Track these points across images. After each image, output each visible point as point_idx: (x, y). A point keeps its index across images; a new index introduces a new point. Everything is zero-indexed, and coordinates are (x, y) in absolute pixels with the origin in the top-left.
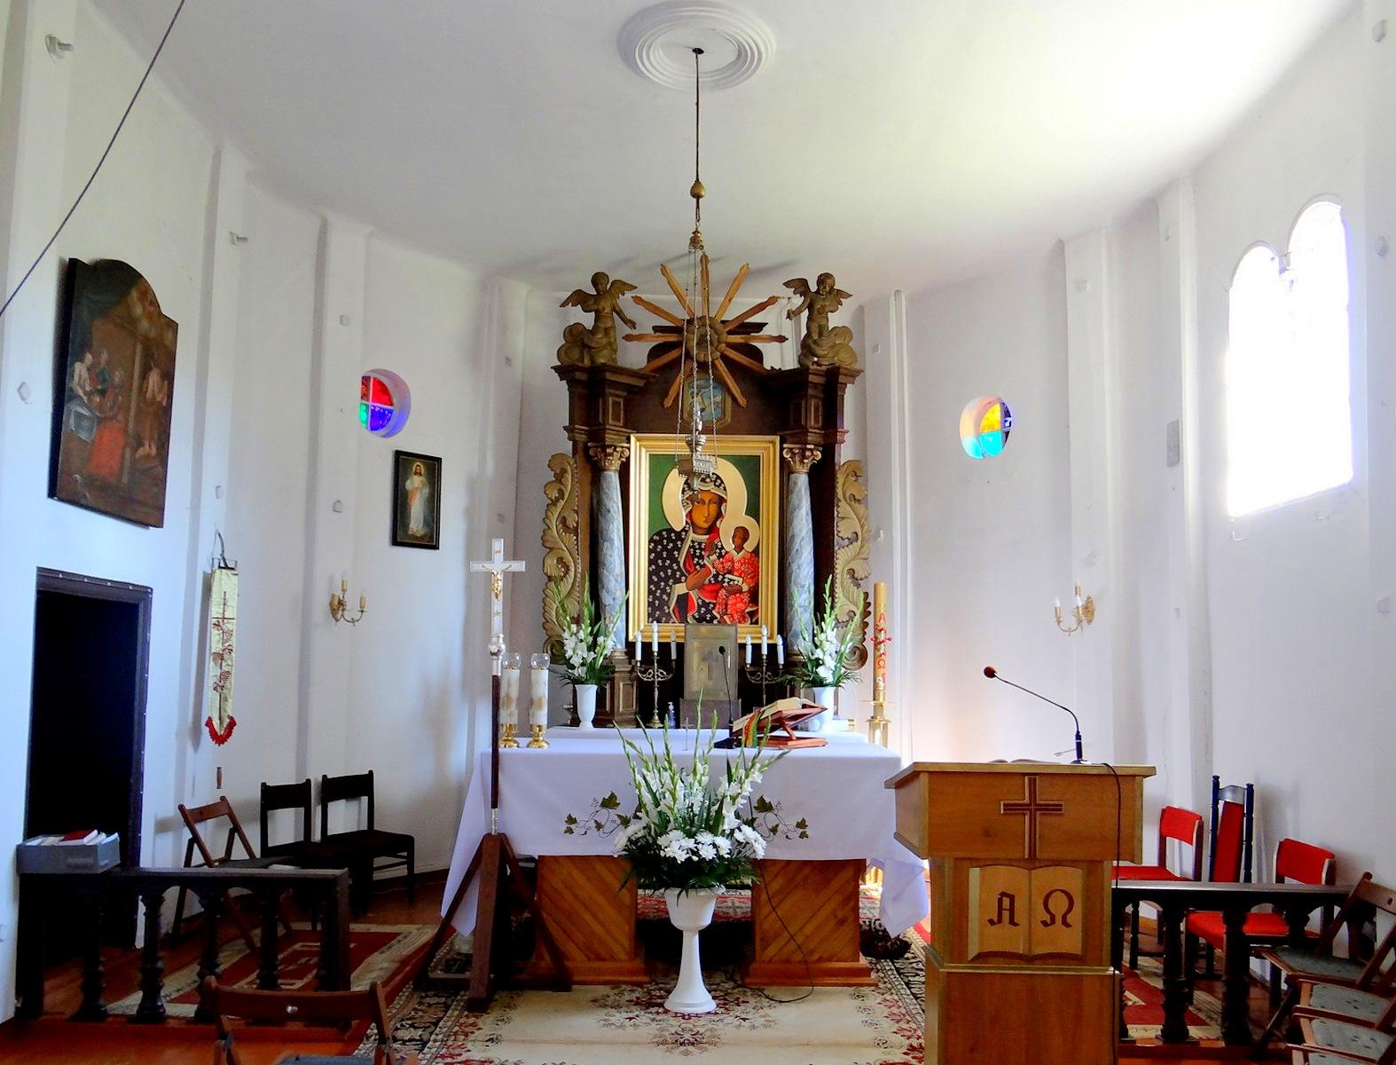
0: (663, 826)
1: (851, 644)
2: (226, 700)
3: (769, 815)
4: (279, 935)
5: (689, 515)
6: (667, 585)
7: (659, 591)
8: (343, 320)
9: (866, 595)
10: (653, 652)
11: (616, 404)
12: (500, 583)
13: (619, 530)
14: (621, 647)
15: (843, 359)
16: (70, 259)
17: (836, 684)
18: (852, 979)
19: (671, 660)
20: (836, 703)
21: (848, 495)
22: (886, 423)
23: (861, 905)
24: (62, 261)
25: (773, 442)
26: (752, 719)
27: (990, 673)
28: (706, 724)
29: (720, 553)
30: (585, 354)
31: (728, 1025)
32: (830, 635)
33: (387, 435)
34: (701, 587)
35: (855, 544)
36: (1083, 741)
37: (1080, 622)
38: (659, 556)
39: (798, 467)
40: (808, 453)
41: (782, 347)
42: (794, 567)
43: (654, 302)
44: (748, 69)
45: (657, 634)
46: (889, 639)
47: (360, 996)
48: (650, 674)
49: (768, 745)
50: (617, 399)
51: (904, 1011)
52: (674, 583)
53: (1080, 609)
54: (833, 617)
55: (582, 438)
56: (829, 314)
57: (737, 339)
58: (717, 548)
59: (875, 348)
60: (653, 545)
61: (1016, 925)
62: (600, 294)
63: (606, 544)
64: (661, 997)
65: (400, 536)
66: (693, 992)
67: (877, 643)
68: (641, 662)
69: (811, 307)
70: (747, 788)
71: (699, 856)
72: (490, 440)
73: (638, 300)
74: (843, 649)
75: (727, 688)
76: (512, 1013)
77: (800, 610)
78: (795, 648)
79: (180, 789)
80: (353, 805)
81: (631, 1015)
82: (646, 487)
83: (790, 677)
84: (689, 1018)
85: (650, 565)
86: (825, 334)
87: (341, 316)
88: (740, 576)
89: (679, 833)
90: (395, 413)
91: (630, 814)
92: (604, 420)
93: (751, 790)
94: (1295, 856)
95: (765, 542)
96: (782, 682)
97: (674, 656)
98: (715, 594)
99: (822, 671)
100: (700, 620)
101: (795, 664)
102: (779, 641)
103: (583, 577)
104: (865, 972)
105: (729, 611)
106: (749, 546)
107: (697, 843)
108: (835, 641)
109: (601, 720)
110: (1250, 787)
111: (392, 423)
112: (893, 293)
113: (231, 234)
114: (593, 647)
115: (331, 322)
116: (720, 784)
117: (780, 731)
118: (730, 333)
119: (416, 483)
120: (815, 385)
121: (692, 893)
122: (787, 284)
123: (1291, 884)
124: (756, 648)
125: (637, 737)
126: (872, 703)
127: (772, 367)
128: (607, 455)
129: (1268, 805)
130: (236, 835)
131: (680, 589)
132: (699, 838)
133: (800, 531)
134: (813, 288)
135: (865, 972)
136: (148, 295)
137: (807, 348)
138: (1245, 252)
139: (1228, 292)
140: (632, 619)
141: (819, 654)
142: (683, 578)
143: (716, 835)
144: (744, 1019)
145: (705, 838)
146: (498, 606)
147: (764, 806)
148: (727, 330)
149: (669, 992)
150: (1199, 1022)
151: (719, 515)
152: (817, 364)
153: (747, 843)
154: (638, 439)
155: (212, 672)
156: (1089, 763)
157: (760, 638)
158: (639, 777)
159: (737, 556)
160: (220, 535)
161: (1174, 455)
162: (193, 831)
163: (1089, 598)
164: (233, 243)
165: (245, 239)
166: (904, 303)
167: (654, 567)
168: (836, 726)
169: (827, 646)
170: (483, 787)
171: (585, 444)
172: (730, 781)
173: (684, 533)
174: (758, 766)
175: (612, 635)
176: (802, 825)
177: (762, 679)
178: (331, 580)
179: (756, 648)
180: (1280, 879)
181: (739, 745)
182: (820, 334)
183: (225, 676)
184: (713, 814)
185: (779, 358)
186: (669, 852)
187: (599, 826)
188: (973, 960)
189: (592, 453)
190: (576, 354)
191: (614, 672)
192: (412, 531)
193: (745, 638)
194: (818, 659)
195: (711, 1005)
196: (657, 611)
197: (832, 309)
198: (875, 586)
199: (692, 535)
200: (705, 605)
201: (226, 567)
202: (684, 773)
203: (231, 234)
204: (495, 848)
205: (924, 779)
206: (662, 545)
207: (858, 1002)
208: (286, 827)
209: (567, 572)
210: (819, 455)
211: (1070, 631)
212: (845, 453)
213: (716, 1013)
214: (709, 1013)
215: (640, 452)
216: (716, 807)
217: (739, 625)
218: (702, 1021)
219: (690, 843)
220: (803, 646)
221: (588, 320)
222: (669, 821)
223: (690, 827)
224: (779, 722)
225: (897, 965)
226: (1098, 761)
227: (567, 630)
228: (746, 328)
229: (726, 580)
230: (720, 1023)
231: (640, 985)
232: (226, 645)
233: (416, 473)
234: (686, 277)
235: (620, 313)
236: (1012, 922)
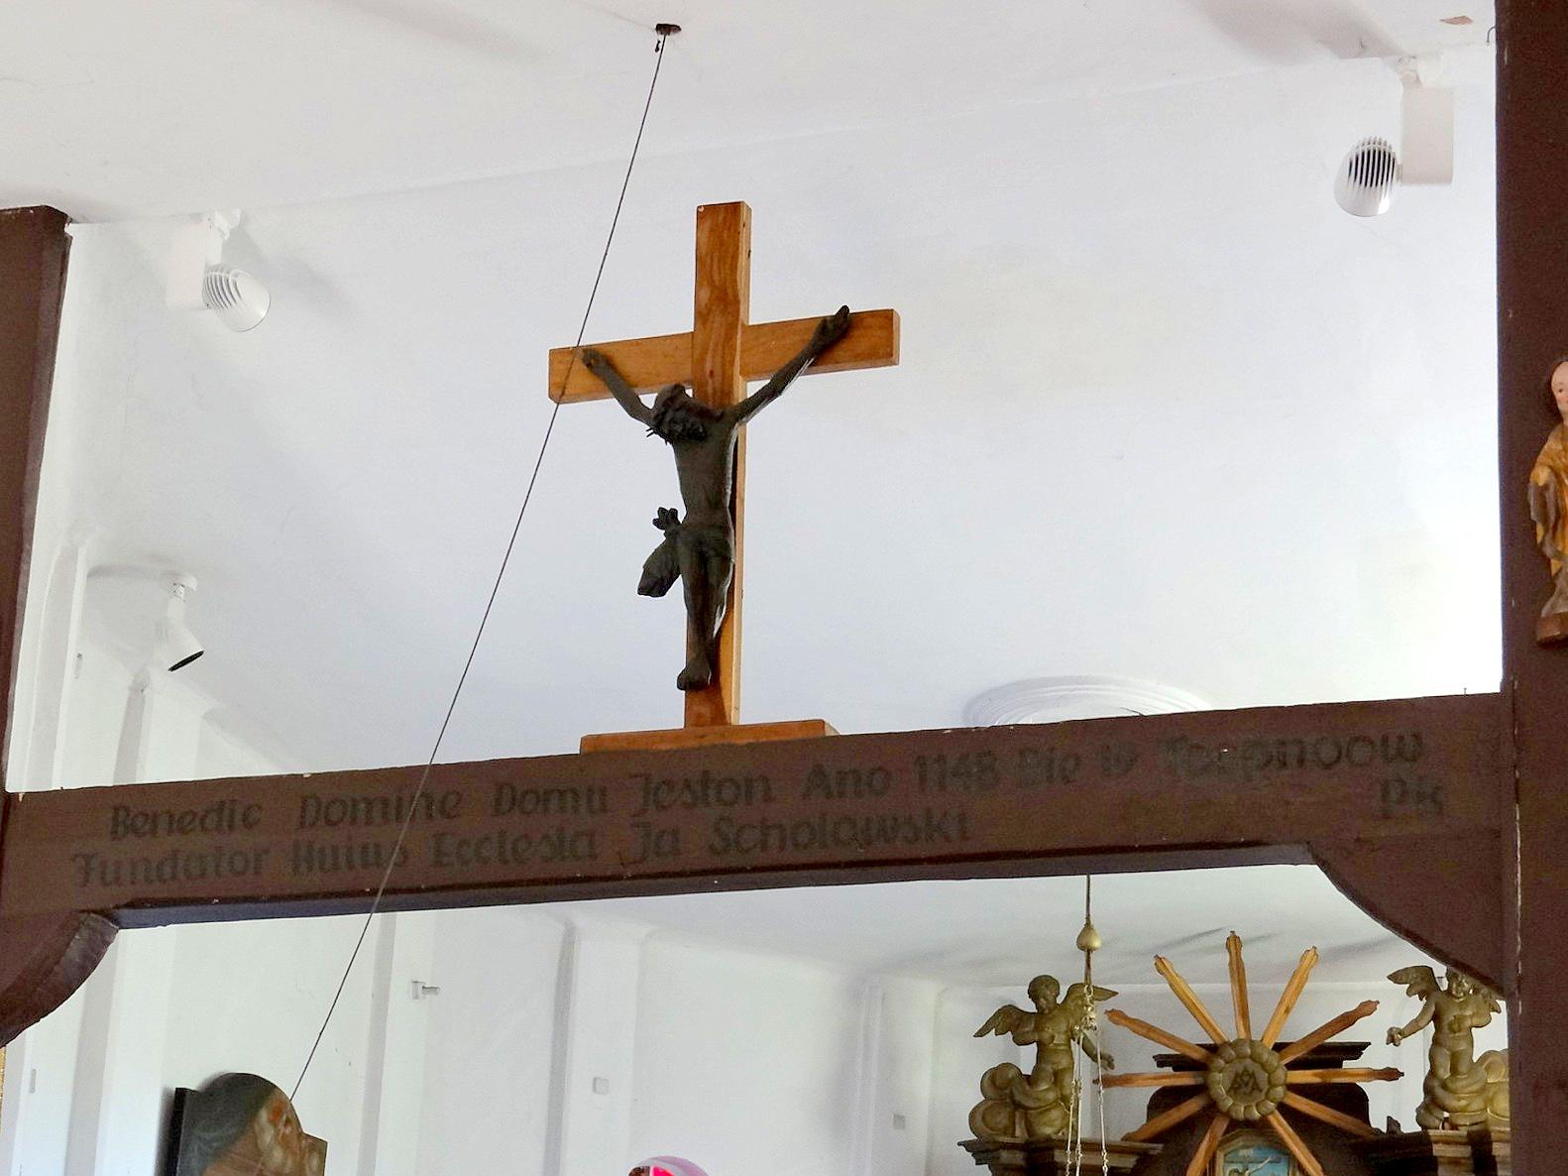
4: (691, 395)
16: (177, 1089)
24: (166, 1093)
56: (1473, 1029)
73: (1116, 1016)
86: (1463, 1068)
87: (595, 1079)
115: (578, 1096)
120: (1455, 1162)
122: (1396, 977)
136: (283, 1112)
152: (1454, 1127)
164: (417, 997)
165: (434, 989)
182: (1454, 1070)
185: (1393, 1106)
190: (1002, 1119)
197: (1475, 1021)
221: (1026, 1059)
228: (1327, 1054)
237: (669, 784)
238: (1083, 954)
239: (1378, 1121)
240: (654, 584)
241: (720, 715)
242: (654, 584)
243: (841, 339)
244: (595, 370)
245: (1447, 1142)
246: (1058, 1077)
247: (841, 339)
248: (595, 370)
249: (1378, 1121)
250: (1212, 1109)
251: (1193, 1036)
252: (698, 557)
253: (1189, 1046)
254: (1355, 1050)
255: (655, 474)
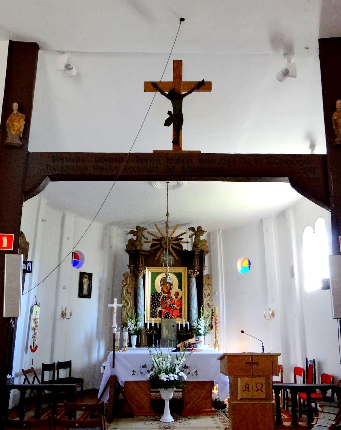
0: (160, 373)
1: (208, 324)
2: (35, 340)
3: (188, 370)
5: (162, 289)
6: (156, 307)
7: (154, 309)
8: (68, 238)
9: (212, 310)
10: (152, 326)
11: (142, 260)
12: (116, 310)
13: (142, 293)
14: (143, 325)
15: (204, 248)
17: (204, 335)
18: (211, 414)
19: (157, 329)
20: (205, 340)
21: (206, 283)
22: (217, 264)
23: (212, 395)
25: (186, 269)
26: (182, 344)
27: (242, 332)
28: (170, 347)
29: (171, 299)
30: (134, 246)
31: (178, 424)
32: (202, 322)
33: (78, 268)
34: (165, 308)
35: (209, 296)
36: (264, 348)
37: (271, 317)
38: (154, 300)
39: (193, 276)
40: (195, 272)
41: (187, 245)
42: (192, 303)
43: (153, 232)
44: (180, 186)
45: (153, 321)
46: (219, 322)
47: (100, 404)
48: (151, 332)
49: (187, 351)
50: (143, 258)
51: (224, 421)
52: (158, 307)
53: (271, 315)
54: (203, 316)
55: (132, 268)
57: (176, 242)
58: (170, 297)
59: (213, 244)
60: (152, 297)
61: (249, 391)
62: (138, 231)
63: (139, 297)
64: (159, 419)
65: (81, 295)
66: (168, 417)
67: (216, 323)
68: (149, 329)
69: (195, 235)
70: (182, 362)
71: (170, 379)
72: (106, 268)
73: (148, 232)
74: (206, 325)
75: (173, 336)
76: (118, 423)
77: (194, 314)
78: (193, 325)
79: (21, 365)
80: (65, 370)
81: (151, 422)
82: (150, 280)
83: (191, 333)
84: (167, 423)
85: (151, 302)
88: (177, 305)
89: (164, 374)
90: (80, 262)
91: (150, 369)
92: (139, 263)
93: (183, 362)
94: (325, 377)
95: (183, 295)
96: (189, 334)
97: (158, 327)
98: (170, 310)
99: (200, 331)
100: (165, 317)
101: (193, 329)
102: (188, 323)
103: (133, 305)
104: (214, 412)
105: (174, 315)
106: (179, 297)
107: (169, 376)
108: (204, 323)
109: (138, 345)
110: (314, 361)
111: (79, 264)
112: (218, 230)
113: (42, 219)
114: (136, 325)
116: (174, 361)
117: (190, 347)
118: (173, 241)
119: (85, 281)
120: (197, 255)
121: (168, 390)
122: (189, 229)
123: (324, 384)
124: (182, 325)
125: (153, 350)
126: (215, 340)
127: (185, 249)
128: (139, 273)
129: (319, 365)
130: (26, 381)
131: (160, 309)
132: (170, 375)
133: (194, 293)
134: (196, 230)
135: (214, 412)
136: (24, 237)
137: (195, 245)
138: (306, 227)
139: (302, 235)
140: (146, 317)
141: (199, 326)
142: (161, 306)
143: (174, 374)
144: (182, 423)
145: (171, 375)
146: (115, 315)
147: (186, 367)
148: (173, 240)
149: (161, 417)
150: (302, 421)
151: (171, 289)
152: (198, 250)
153: (182, 376)
154: (148, 268)
155: (32, 333)
156: (265, 353)
157: (183, 322)
158: (153, 359)
159: (176, 300)
160: (35, 297)
161: (292, 275)
162: (26, 376)
163: (273, 311)
164: (42, 221)
165: (46, 220)
166: (221, 232)
167: (152, 303)
168: (205, 346)
169: (202, 324)
170: (110, 362)
171: (133, 270)
172: (177, 360)
173: (161, 294)
174: (184, 356)
175: (141, 322)
176: (196, 372)
177: (152, 333)
178: (62, 307)
179: (182, 325)
180: (322, 383)
181: (179, 351)
183: (35, 334)
184: (173, 369)
185: (187, 247)
186: (162, 378)
187: (141, 373)
188: (239, 400)
189: (135, 272)
191: (141, 332)
192: (84, 293)
193: (178, 322)
194: (199, 328)
195: (173, 420)
196: (153, 315)
198: (215, 308)
199: (163, 294)
200: (167, 313)
201: (37, 305)
202: (165, 358)
203: (42, 219)
204: (113, 380)
205: (226, 357)
206: (155, 297)
207: (212, 419)
208: (47, 376)
209: (128, 304)
210: (198, 273)
211: (268, 320)
212: (206, 272)
213: (174, 422)
214: (172, 422)
215: (148, 272)
216: (174, 367)
217: (177, 318)
218: (171, 423)
219: (167, 376)
220: (195, 324)
221: (135, 238)
222: (161, 371)
223: (167, 372)
224: (190, 345)
225: (223, 411)
226: (268, 352)
227: (128, 320)
228: (178, 239)
229: (173, 306)
230: (176, 424)
231: (153, 416)
232: (36, 325)
233: (85, 278)
234: (162, 227)
235: (143, 236)
236: (248, 391)
237: (172, 159)
238: (167, 217)
239: (184, 249)
240: (167, 124)
241: (180, 148)
242: (167, 124)
243: (203, 86)
244: (153, 87)
245: (197, 252)
246: (140, 240)
247: (203, 86)
248: (153, 87)
249: (184, 249)
250: (161, 247)
251: (160, 236)
252: (175, 120)
253: (159, 237)
254: (181, 239)
255: (168, 105)
